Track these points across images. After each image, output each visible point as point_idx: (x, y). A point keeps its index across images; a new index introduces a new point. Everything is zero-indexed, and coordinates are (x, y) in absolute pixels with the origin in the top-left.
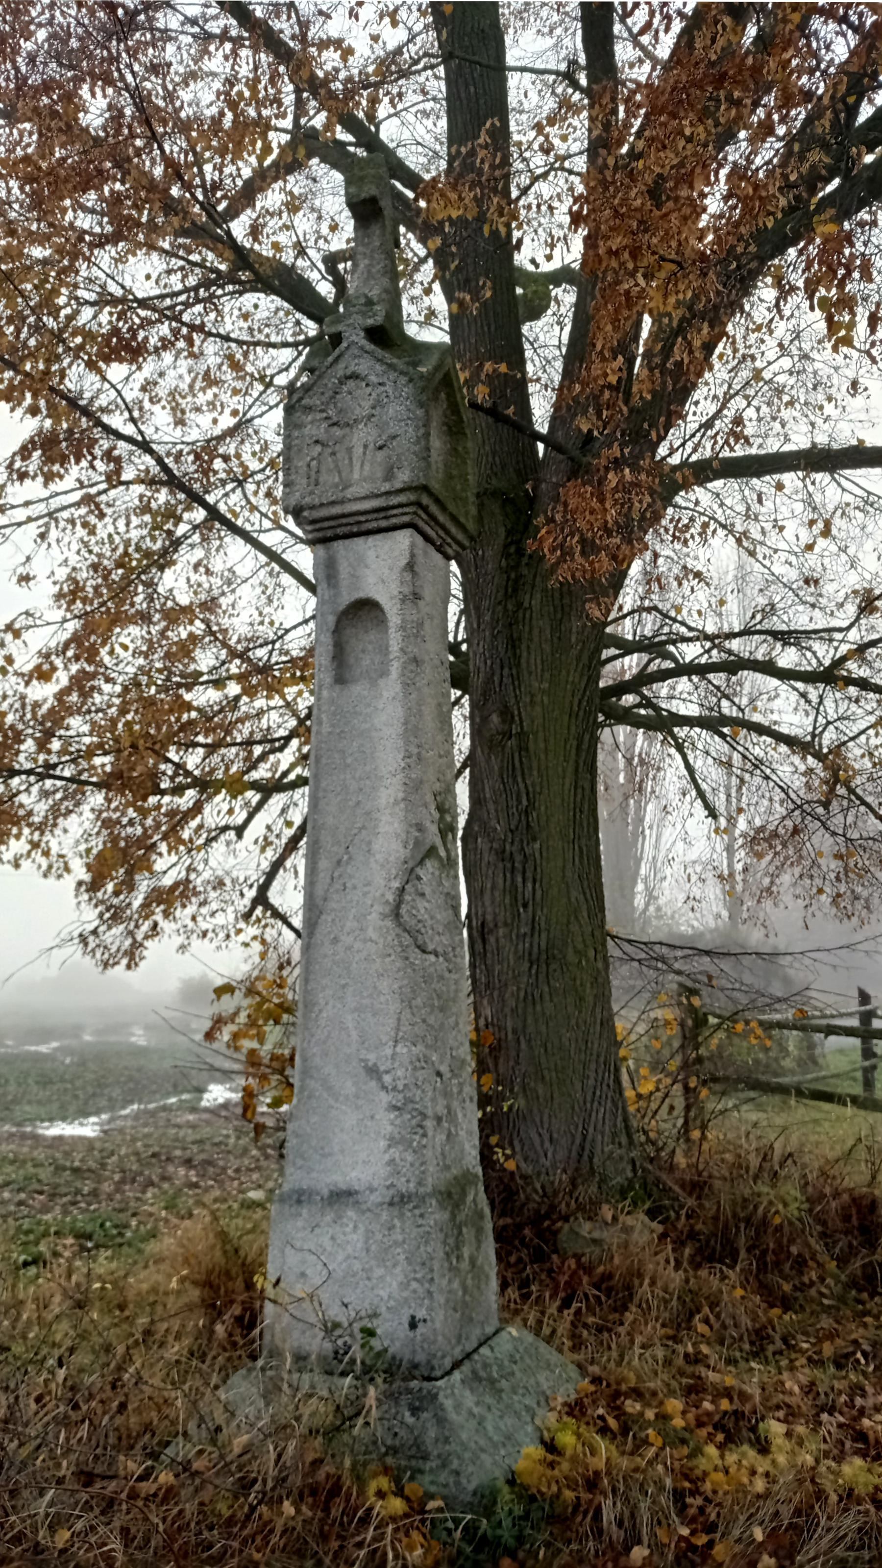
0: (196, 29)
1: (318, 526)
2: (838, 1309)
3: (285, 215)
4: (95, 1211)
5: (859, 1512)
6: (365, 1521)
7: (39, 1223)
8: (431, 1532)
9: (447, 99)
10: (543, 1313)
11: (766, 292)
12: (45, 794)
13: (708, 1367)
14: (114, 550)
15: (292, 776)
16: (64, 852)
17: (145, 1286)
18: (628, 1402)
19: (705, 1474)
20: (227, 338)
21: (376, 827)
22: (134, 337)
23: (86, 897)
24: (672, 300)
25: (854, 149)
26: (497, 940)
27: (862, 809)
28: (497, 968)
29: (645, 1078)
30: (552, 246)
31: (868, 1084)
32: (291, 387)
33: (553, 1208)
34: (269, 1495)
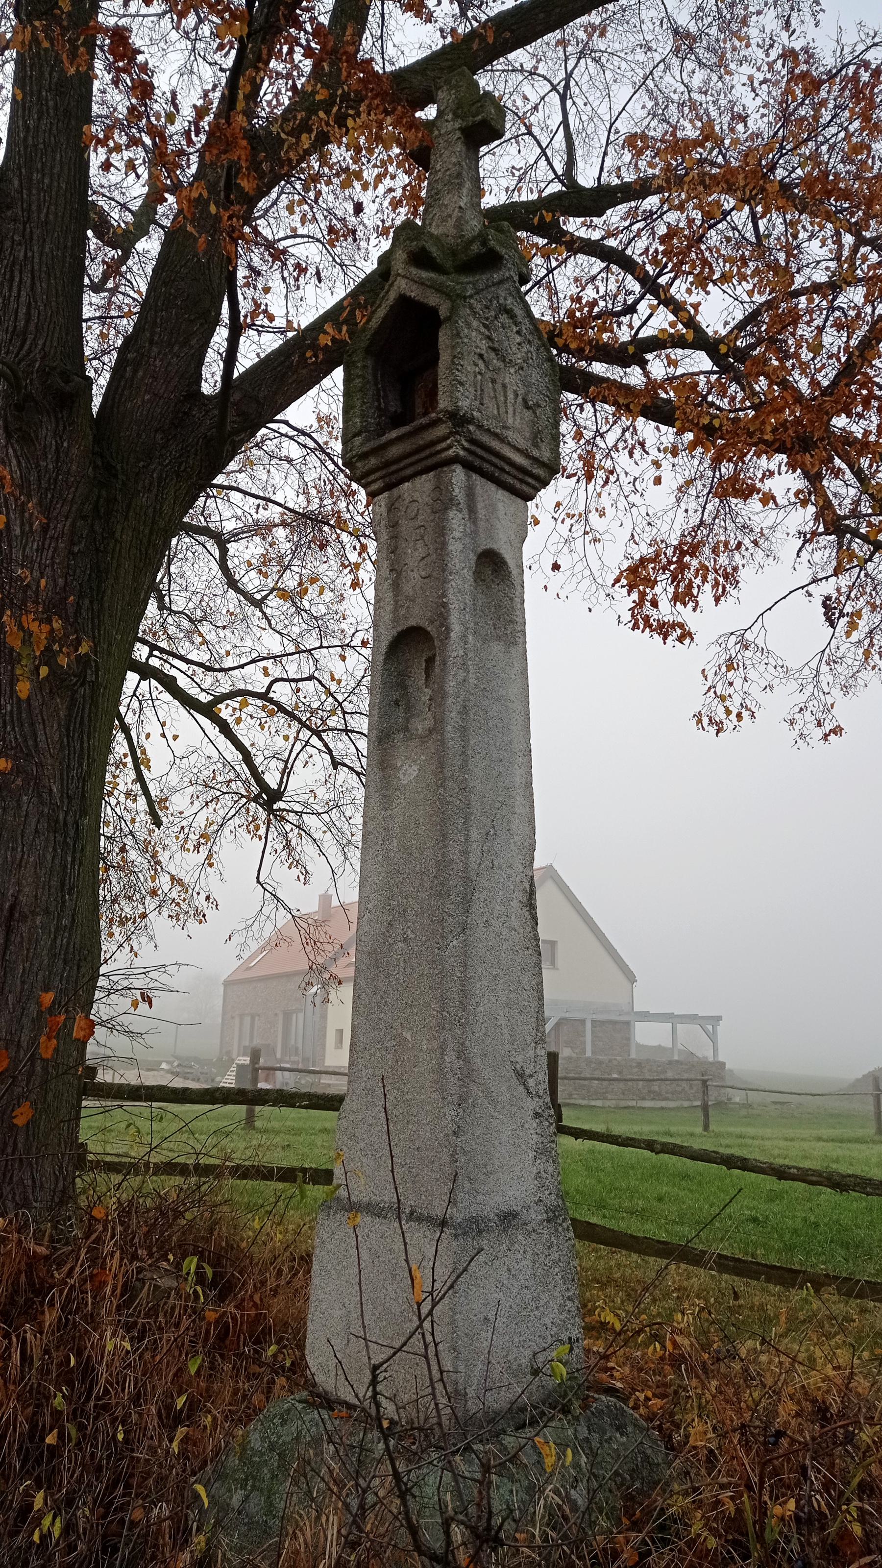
1: (473, 448)
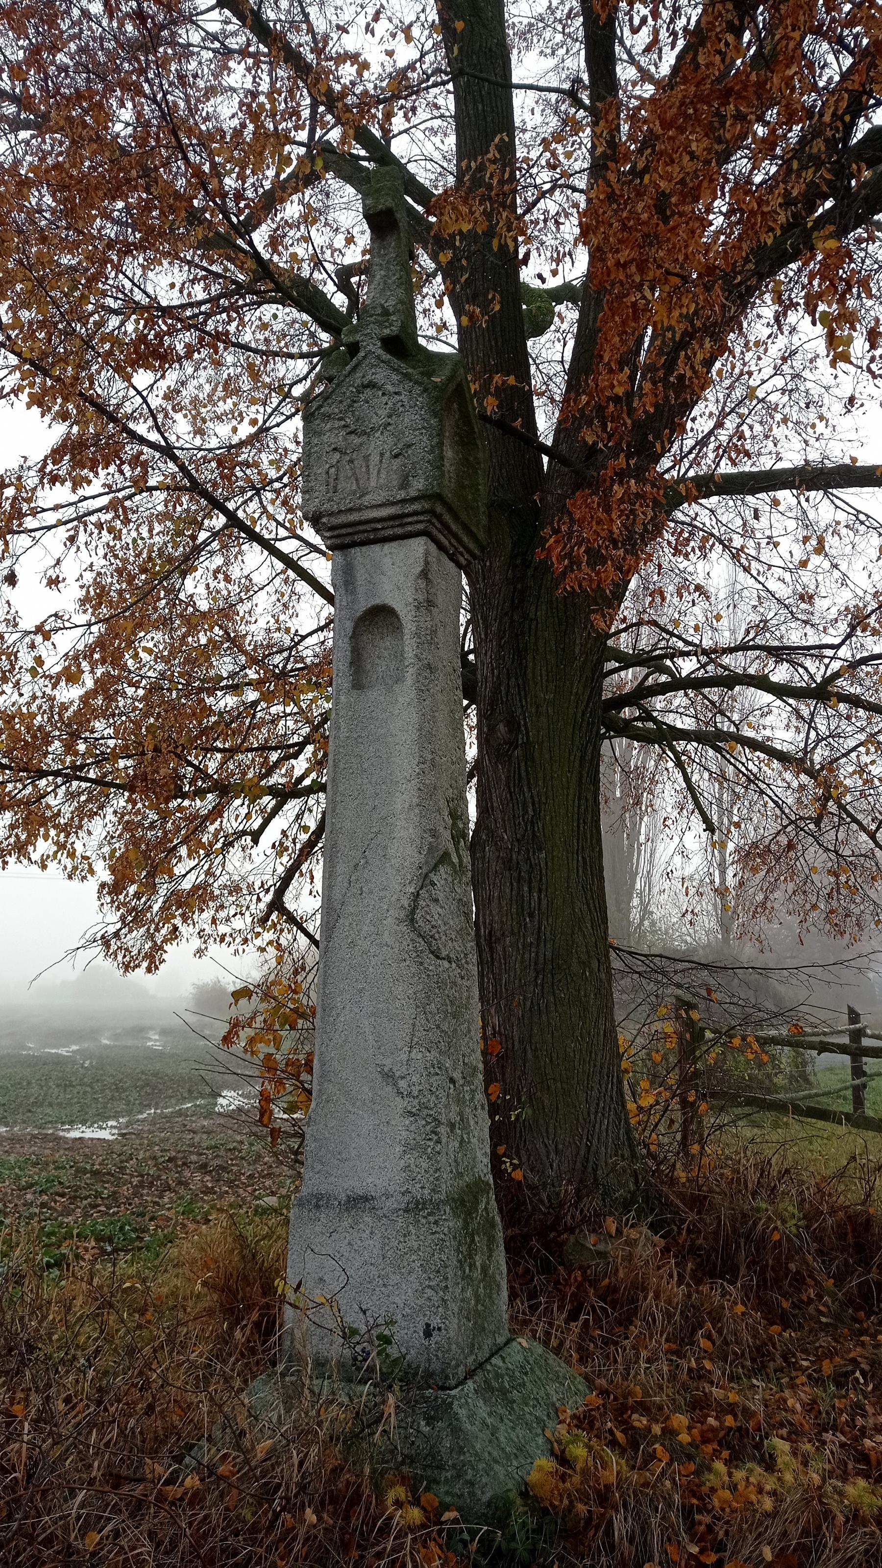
0: (217, 45)
1: (336, 533)
2: (836, 1327)
3: (302, 227)
4: (114, 1214)
5: (866, 1534)
6: (385, 1530)
7: (60, 1226)
8: (447, 1544)
9: (457, 117)
10: (551, 1325)
11: (767, 309)
12: (71, 796)
13: (712, 1383)
14: (138, 556)
15: (307, 782)
16: (88, 854)
17: (165, 1290)
18: (635, 1416)
19: (713, 1490)
20: (246, 347)
21: (392, 832)
22: (161, 343)
23: (108, 899)
24: (676, 314)
25: (854, 166)
26: (504, 950)
27: (854, 826)
28: (505, 976)
29: (647, 1091)
30: (558, 261)
31: (858, 1101)
32: (306, 397)
33: (558, 1218)
34: (293, 1500)
